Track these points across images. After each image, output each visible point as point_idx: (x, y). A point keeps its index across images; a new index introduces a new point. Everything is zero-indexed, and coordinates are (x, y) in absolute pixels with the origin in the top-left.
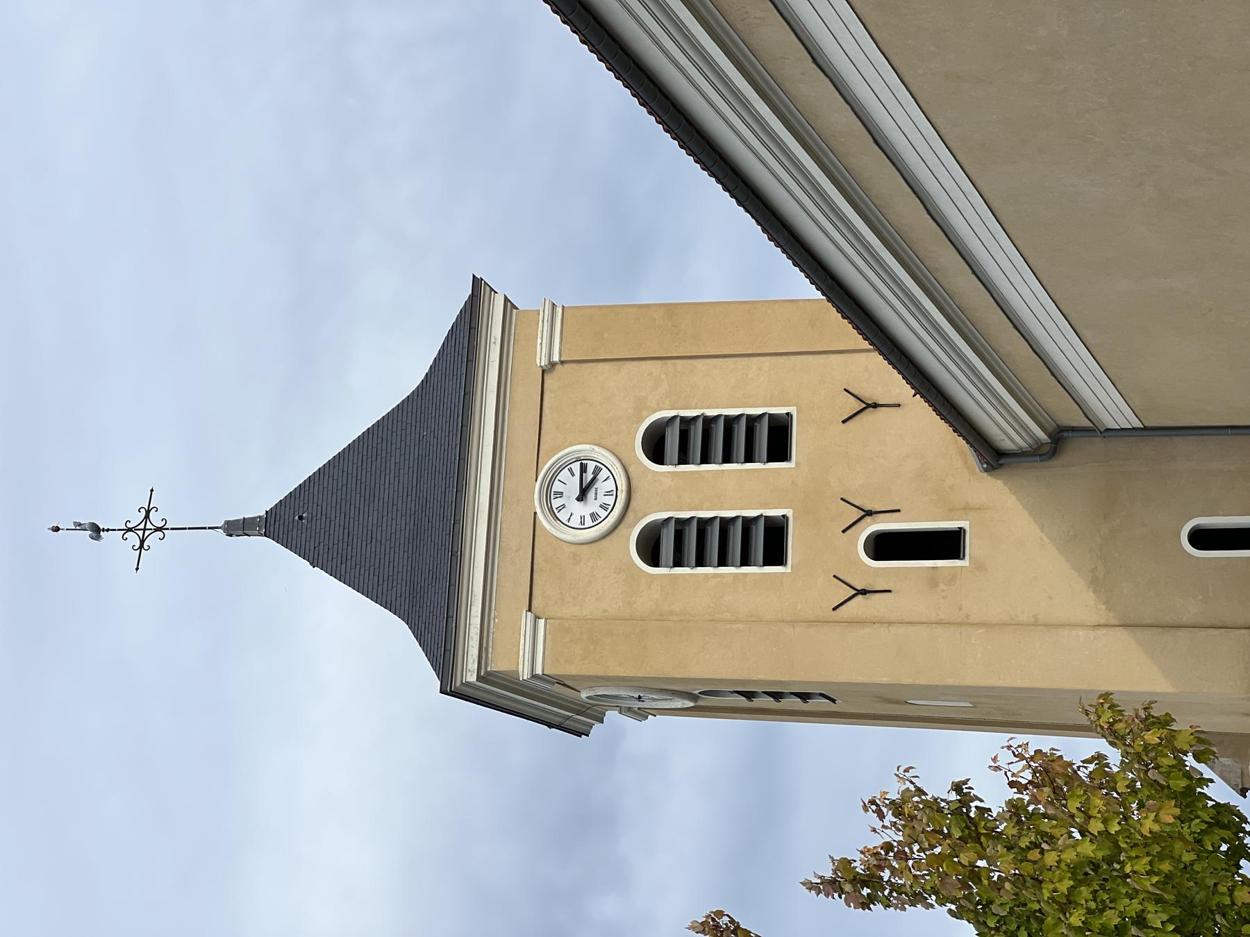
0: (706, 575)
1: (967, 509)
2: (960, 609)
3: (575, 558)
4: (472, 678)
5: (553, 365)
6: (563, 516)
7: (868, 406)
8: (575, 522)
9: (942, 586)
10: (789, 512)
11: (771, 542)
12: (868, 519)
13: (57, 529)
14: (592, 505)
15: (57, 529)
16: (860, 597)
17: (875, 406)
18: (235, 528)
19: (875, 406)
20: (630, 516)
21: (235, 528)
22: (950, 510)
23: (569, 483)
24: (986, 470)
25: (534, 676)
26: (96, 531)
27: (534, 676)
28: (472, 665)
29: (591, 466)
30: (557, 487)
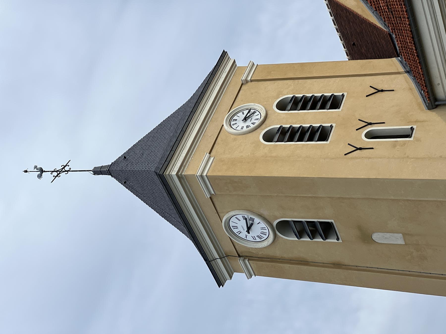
0: (291, 145)
1: (416, 122)
2: (405, 154)
3: (235, 140)
4: (174, 173)
5: (247, 82)
6: (234, 127)
7: (379, 91)
8: (239, 128)
9: (398, 147)
10: (333, 221)
11: (323, 134)
12: (370, 126)
13: (26, 171)
14: (248, 123)
15: (26, 171)
16: (358, 151)
17: (382, 91)
18: (98, 171)
19: (382, 91)
20: (264, 126)
21: (98, 171)
22: (409, 122)
23: (241, 116)
24: (429, 109)
25: (202, 176)
26: (42, 171)
27: (202, 176)
28: (176, 169)
29: (252, 111)
30: (235, 118)
